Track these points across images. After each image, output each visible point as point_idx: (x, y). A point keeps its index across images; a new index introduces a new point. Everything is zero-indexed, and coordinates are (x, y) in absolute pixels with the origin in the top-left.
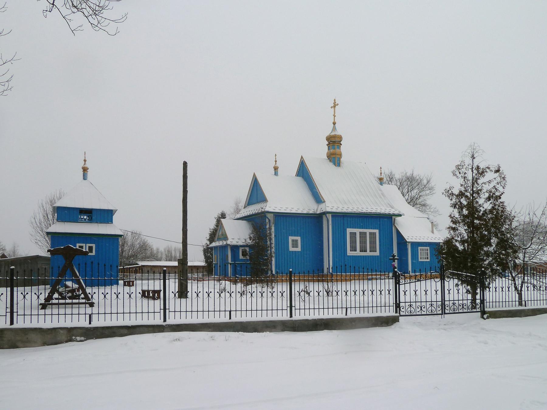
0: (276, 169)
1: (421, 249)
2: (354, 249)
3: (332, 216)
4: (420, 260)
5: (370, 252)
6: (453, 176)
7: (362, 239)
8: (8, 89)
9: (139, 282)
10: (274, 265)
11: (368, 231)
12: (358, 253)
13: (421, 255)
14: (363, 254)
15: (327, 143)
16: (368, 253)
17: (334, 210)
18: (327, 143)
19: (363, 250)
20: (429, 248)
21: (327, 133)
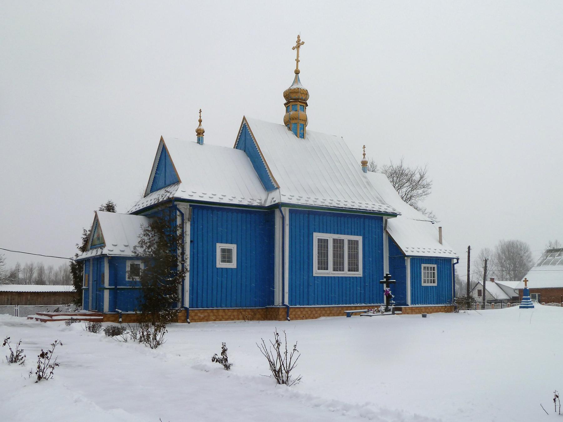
0: (200, 133)
1: (425, 268)
2: (323, 265)
12: (330, 272)
13: (425, 277)
16: (346, 273)
17: (294, 201)
19: (338, 266)
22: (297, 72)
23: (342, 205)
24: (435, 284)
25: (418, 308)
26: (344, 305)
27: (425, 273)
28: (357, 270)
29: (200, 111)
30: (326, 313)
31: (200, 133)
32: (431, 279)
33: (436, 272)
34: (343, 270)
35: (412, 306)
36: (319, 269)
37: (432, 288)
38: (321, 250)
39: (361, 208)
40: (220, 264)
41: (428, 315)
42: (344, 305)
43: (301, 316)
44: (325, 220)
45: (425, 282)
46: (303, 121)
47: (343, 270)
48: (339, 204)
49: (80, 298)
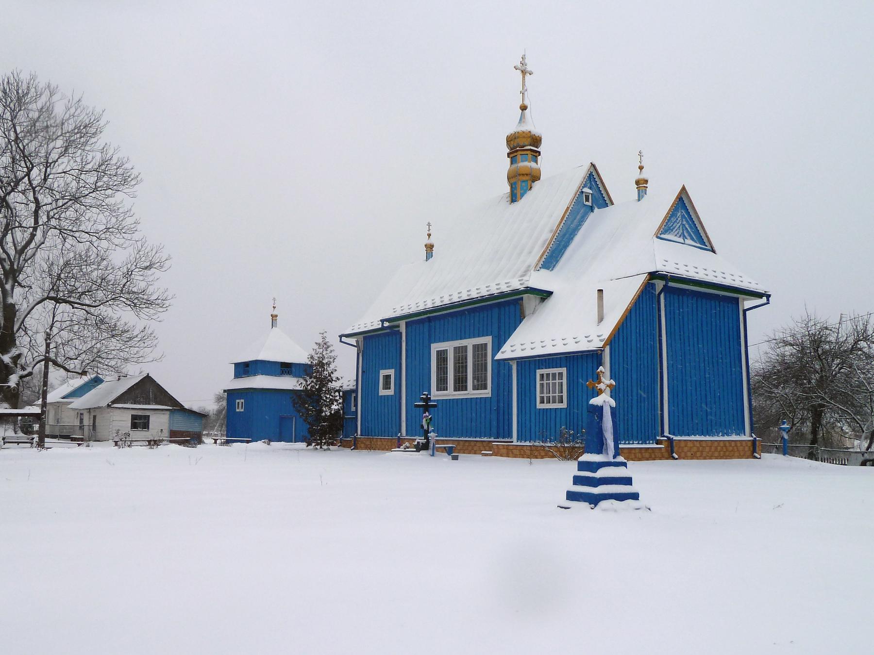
0: (430, 248)
1: (542, 376)
2: (442, 384)
3: (468, 312)
4: (539, 406)
5: (455, 390)
6: (172, 258)
7: (482, 360)
8: (114, 310)
9: (10, 419)
10: (137, 413)
11: (470, 343)
12: (451, 393)
13: (542, 392)
14: (460, 395)
15: (508, 151)
16: (471, 393)
17: (406, 311)
18: (508, 151)
19: (460, 384)
20: (564, 370)
21: (513, 128)
22: (524, 108)
23: (474, 295)
24: (564, 405)
25: (519, 448)
26: (478, 439)
27: (542, 385)
28: (486, 388)
29: (429, 225)
30: (636, 457)
31: (430, 248)
32: (554, 395)
33: (565, 381)
34: (466, 390)
35: (519, 444)
36: (437, 390)
37: (553, 413)
38: (441, 365)
39: (462, 299)
40: (383, 392)
41: (461, 456)
42: (478, 439)
43: (383, 447)
44: (672, 299)
45: (542, 402)
46: (514, 178)
47: (466, 390)
48: (470, 294)
49: (786, 439)
